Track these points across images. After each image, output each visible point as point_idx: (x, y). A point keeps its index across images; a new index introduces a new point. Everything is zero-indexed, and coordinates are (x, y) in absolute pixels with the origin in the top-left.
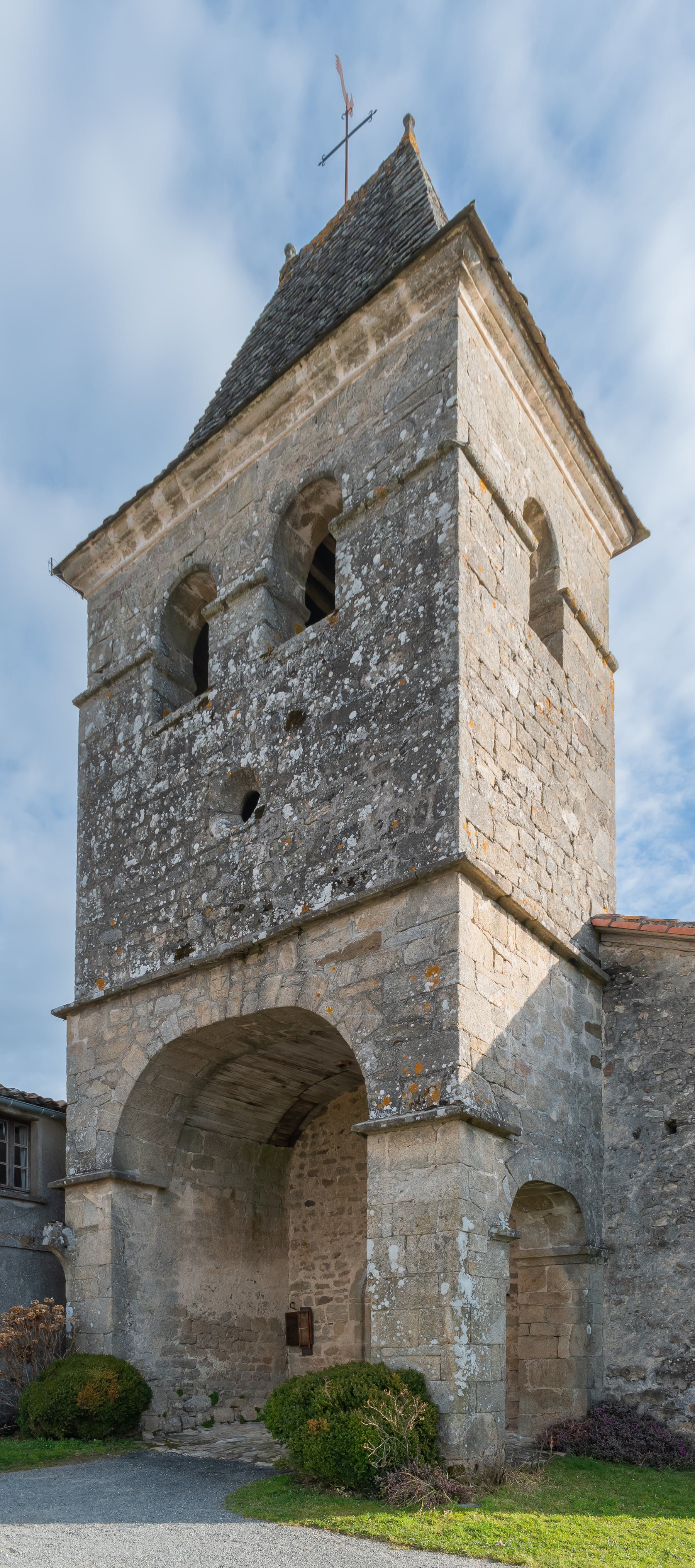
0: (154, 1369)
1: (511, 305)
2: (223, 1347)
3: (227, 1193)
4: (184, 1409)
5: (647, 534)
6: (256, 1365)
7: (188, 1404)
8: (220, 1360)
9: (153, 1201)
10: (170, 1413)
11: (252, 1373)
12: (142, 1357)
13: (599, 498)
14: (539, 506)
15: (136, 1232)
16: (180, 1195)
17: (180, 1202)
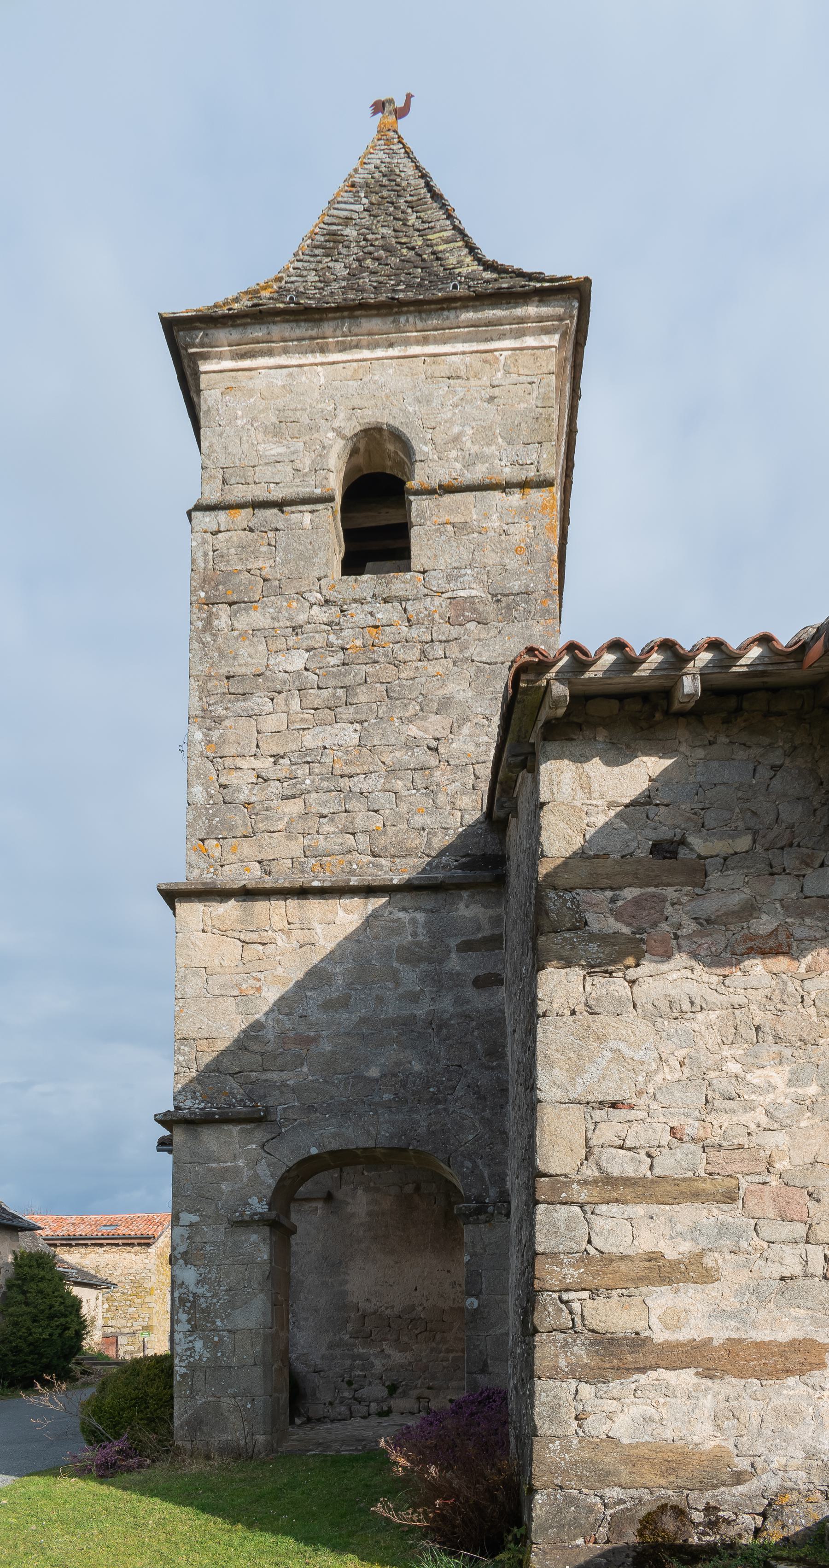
0: (319, 1362)
1: (256, 319)
2: (405, 1339)
3: (409, 1189)
4: (354, 1398)
5: (588, 281)
6: (451, 1356)
7: (358, 1395)
8: (400, 1352)
9: (319, 1212)
10: (337, 1401)
11: (444, 1364)
12: (305, 1351)
13: (489, 323)
14: (374, 429)
15: (299, 1241)
16: (350, 1200)
17: (350, 1206)
